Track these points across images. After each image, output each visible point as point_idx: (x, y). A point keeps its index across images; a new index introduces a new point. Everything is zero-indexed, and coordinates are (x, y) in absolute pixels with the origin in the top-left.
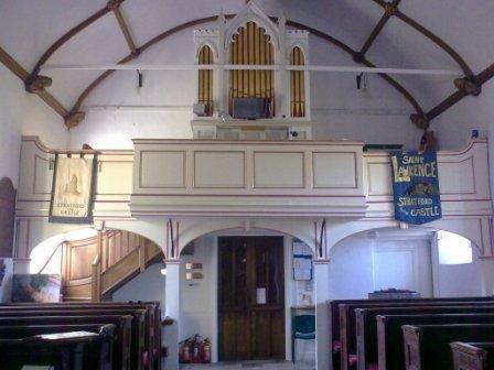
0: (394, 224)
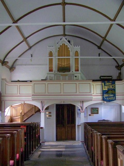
0: (102, 102)
